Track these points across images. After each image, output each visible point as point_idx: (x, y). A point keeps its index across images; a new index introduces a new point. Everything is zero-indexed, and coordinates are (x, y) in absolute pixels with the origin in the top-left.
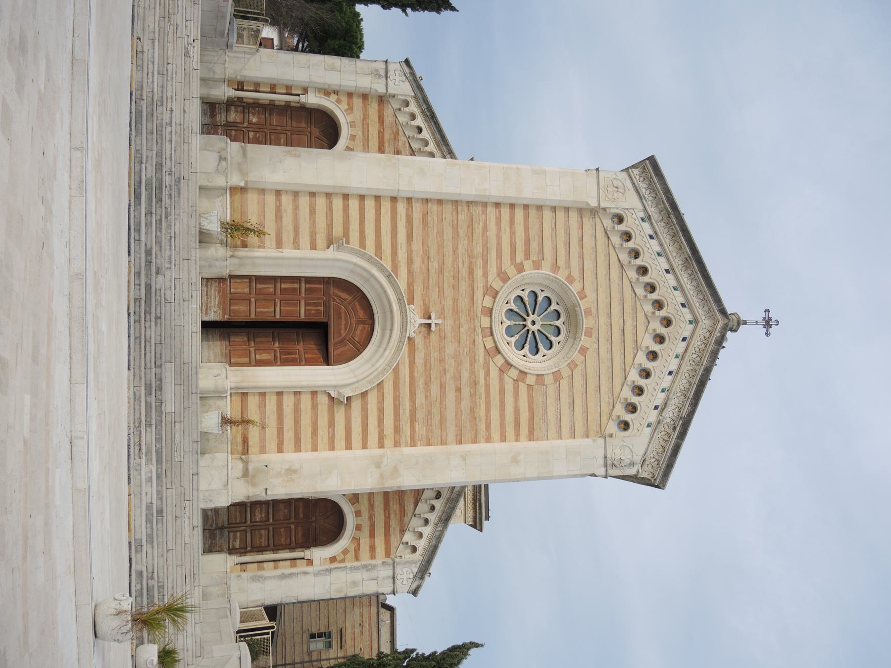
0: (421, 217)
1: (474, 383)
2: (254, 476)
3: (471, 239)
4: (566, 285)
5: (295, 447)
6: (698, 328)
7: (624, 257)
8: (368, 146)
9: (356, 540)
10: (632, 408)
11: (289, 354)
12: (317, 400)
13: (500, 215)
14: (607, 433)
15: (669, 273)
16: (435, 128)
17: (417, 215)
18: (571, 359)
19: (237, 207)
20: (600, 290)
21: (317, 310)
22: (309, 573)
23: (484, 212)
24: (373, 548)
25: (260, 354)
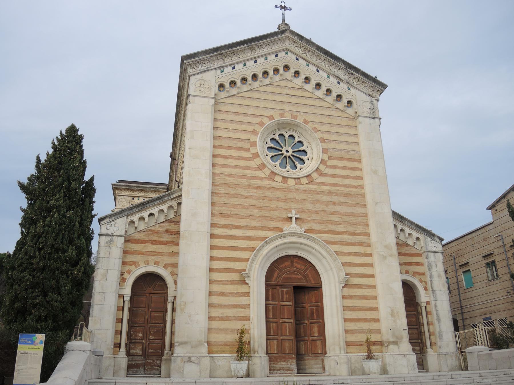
0: (223, 218)
1: (330, 193)
2: (397, 338)
3: (237, 186)
4: (266, 127)
5: (375, 311)
6: (291, 49)
7: (245, 88)
8: (162, 252)
9: (415, 274)
10: (339, 97)
11: (312, 313)
12: (347, 296)
13: (220, 164)
14: (354, 115)
15: (256, 61)
16: (151, 204)
17: (223, 221)
18: (312, 130)
19: (221, 348)
20: (267, 106)
21: (286, 293)
22: (436, 304)
23: (219, 175)
24: (418, 264)
25: (314, 333)
